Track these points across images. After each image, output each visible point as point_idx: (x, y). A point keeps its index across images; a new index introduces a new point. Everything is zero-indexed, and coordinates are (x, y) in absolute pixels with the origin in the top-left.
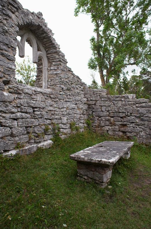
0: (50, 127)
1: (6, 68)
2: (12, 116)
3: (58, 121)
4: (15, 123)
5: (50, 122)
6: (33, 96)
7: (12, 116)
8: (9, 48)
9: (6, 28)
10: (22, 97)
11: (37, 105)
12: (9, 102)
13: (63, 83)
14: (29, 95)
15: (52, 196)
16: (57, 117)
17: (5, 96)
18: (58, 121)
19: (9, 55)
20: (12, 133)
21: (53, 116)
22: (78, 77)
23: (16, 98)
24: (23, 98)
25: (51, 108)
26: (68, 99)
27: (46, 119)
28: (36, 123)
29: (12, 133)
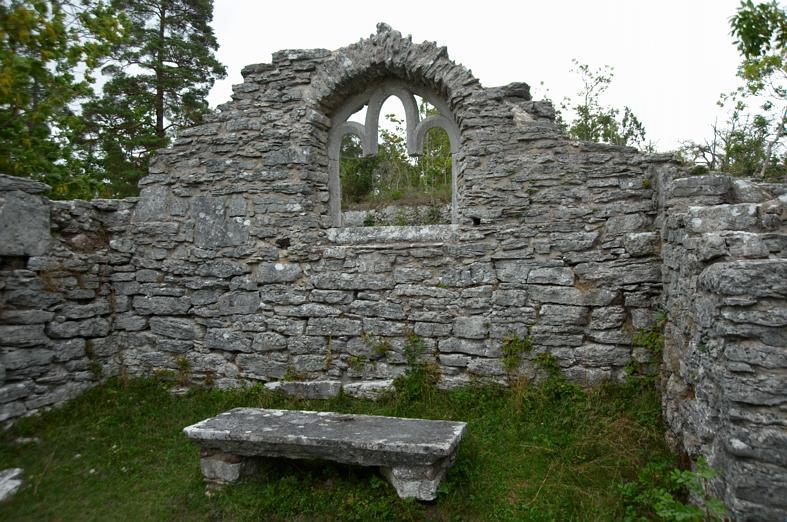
0: (398, 343)
1: (281, 215)
2: (292, 310)
3: (434, 327)
4: (299, 326)
5: (400, 329)
6: (349, 263)
7: (292, 310)
8: (290, 168)
9: (280, 131)
10: (320, 268)
11: (357, 284)
12: (287, 283)
13: (481, 199)
14: (340, 262)
15: (388, 515)
16: (428, 315)
17: (276, 271)
18: (434, 327)
19: (288, 186)
20: (129, 296)
21: (417, 313)
22: (280, 57)
23: (309, 270)
24: (324, 271)
25: (418, 289)
26: (504, 250)
27: (387, 319)
28: (353, 327)
29: (129, 296)
